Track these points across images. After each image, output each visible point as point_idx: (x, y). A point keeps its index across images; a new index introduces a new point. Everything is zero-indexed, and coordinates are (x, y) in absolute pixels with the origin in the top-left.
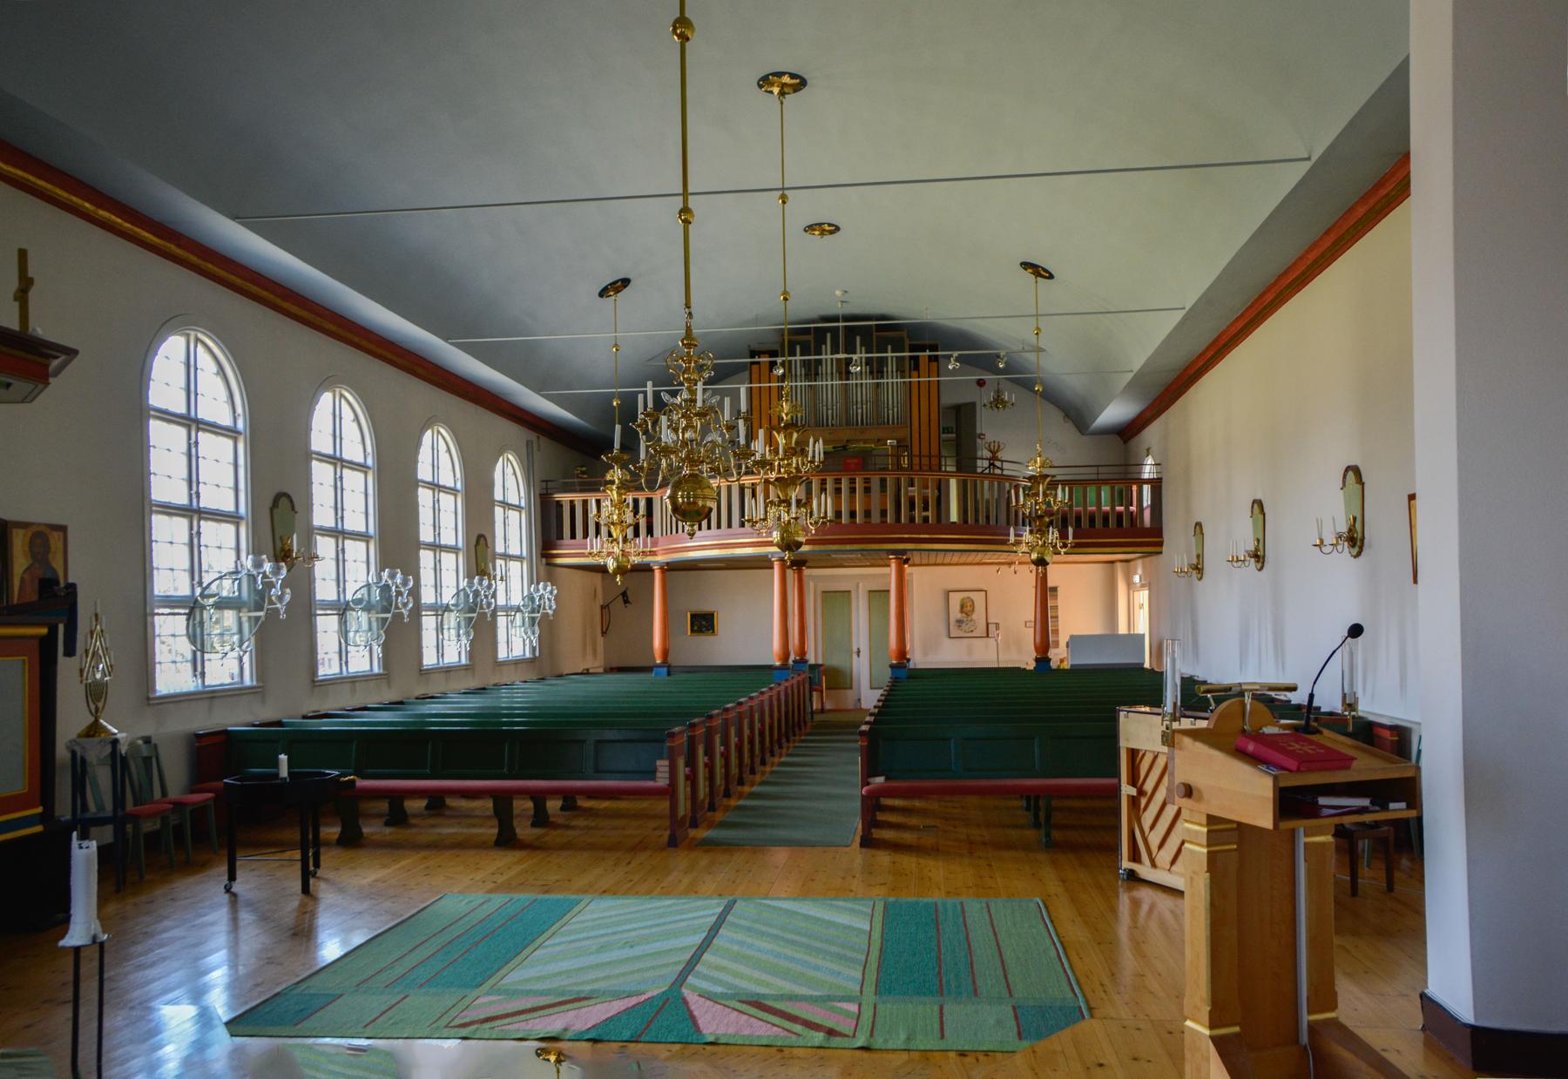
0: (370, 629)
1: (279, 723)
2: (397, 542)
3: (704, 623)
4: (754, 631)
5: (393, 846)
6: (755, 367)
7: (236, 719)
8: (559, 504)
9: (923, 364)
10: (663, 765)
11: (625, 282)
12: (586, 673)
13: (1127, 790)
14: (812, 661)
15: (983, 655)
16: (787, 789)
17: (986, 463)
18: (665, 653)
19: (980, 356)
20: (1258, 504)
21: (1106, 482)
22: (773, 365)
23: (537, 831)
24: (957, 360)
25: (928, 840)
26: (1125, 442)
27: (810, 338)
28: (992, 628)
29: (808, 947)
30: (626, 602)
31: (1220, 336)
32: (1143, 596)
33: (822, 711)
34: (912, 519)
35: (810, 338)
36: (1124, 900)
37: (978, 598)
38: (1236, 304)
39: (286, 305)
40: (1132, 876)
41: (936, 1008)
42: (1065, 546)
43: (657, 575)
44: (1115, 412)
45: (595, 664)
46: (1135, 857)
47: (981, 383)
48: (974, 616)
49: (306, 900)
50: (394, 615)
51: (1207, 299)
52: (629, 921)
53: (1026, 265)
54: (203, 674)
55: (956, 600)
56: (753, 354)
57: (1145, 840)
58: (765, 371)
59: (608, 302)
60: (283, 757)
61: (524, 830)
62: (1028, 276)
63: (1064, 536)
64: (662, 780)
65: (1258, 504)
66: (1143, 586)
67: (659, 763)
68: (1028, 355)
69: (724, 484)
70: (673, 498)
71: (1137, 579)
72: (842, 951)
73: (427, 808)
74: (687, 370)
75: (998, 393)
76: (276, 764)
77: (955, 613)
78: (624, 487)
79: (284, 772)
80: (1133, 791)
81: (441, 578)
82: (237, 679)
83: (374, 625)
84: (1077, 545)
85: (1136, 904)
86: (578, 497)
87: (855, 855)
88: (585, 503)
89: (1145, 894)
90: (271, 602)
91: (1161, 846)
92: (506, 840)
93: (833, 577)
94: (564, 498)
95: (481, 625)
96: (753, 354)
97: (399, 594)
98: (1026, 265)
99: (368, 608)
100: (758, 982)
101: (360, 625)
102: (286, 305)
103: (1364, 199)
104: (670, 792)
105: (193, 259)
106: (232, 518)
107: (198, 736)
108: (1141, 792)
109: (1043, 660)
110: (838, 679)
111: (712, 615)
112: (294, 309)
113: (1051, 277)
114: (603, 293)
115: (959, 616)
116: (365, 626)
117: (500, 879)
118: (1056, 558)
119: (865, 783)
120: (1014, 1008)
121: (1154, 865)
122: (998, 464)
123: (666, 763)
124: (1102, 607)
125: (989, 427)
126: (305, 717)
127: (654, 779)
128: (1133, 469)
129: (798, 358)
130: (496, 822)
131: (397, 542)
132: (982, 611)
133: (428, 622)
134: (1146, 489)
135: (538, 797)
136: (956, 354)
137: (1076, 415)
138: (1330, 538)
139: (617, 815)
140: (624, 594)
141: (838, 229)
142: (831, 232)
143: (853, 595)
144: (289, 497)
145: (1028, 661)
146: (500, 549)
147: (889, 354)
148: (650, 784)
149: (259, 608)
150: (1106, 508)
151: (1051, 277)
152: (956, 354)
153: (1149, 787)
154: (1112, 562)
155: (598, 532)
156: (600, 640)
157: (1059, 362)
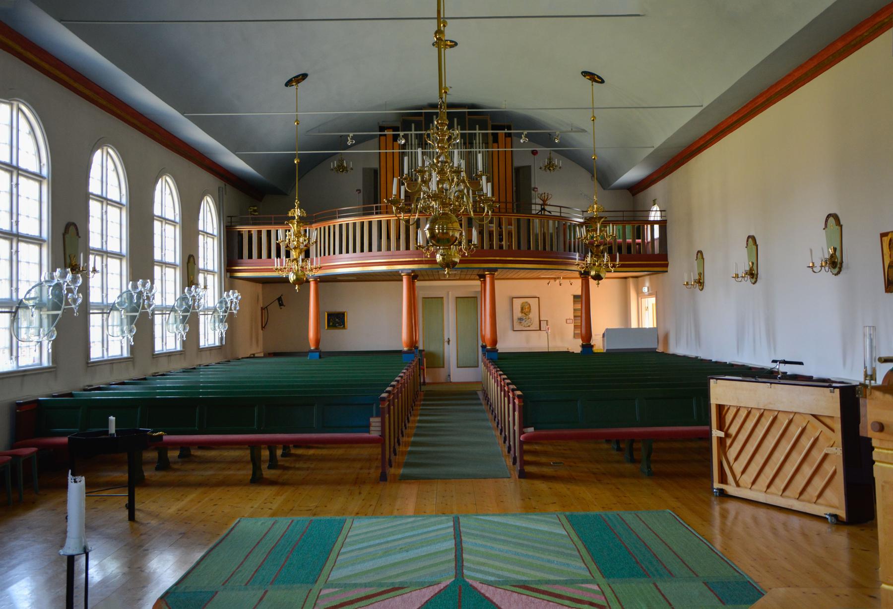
0: (41, 326)
1: (70, 395)
2: (141, 262)
3: (337, 320)
4: (380, 326)
5: (162, 485)
6: (383, 138)
7: (40, 392)
8: (240, 234)
9: (501, 139)
10: (375, 421)
11: (304, 76)
12: (253, 357)
13: (716, 433)
14: (421, 348)
15: (538, 342)
16: (436, 439)
17: (539, 208)
18: (318, 342)
19: (543, 137)
20: (752, 239)
21: (629, 222)
22: (395, 138)
23: (273, 472)
24: (526, 136)
25: (563, 472)
26: (633, 195)
27: (422, 118)
28: (543, 324)
29: (533, 547)
30: (281, 305)
31: (719, 125)
32: (652, 301)
33: (424, 383)
34: (501, 247)
35: (422, 118)
36: (717, 510)
37: (533, 303)
38: (736, 104)
39: (76, 85)
40: (723, 494)
41: (652, 585)
42: (614, 266)
43: (312, 285)
44: (633, 175)
45: (258, 350)
46: (723, 479)
47: (534, 153)
48: (531, 316)
49: (136, 525)
50: (141, 314)
51: (719, 101)
52: (393, 534)
53: (585, 74)
54: (17, 357)
55: (518, 303)
56: (382, 129)
57: (731, 468)
58: (390, 140)
59: (292, 89)
60: (112, 418)
61: (267, 473)
62: (586, 81)
63: (613, 259)
64: (375, 433)
65: (752, 239)
66: (650, 295)
67: (371, 420)
68: (573, 134)
69: (393, 218)
70: (431, 230)
71: (645, 290)
72: (557, 549)
73: (179, 457)
74: (442, 141)
75: (550, 159)
76: (106, 424)
77: (517, 313)
78: (302, 220)
79: (112, 429)
80: (722, 434)
81: (166, 287)
82: (37, 361)
83: (125, 321)
84: (622, 266)
85: (724, 515)
86: (254, 229)
87: (511, 486)
88: (260, 232)
89: (732, 506)
90: (67, 303)
91: (743, 472)
92: (257, 480)
93: (430, 287)
94: (244, 229)
95: (190, 319)
96: (382, 129)
97: (70, 290)
98: (585, 74)
99: (39, 306)
100: (518, 573)
101: (31, 323)
102: (76, 85)
103: (843, 38)
104: (380, 441)
105: (18, 48)
106: (118, 256)
107: (19, 405)
108: (727, 435)
109: (587, 346)
110: (434, 361)
111: (343, 314)
112: (81, 88)
113: (603, 82)
114: (289, 83)
115: (520, 315)
116: (36, 323)
117: (275, 506)
118: (608, 275)
119: (521, 432)
120: (705, 584)
121: (738, 485)
122: (547, 208)
123: (379, 419)
124: (629, 312)
125: (541, 183)
126: (85, 390)
127: (369, 432)
128: (639, 214)
129: (413, 132)
130: (251, 466)
131: (141, 262)
132: (553, 312)
133: (95, 320)
134: (656, 227)
135: (271, 445)
136: (525, 132)
137: (603, 177)
138: (818, 264)
139: (323, 459)
140: (280, 299)
141: (456, 44)
142: (451, 47)
143: (445, 299)
144: (75, 225)
145: (575, 346)
146: (201, 266)
147: (477, 131)
148: (366, 435)
149: (56, 307)
150: (629, 240)
151: (603, 82)
152: (525, 132)
153: (733, 431)
154: (626, 278)
155: (278, 255)
156: (261, 332)
157: (596, 142)
